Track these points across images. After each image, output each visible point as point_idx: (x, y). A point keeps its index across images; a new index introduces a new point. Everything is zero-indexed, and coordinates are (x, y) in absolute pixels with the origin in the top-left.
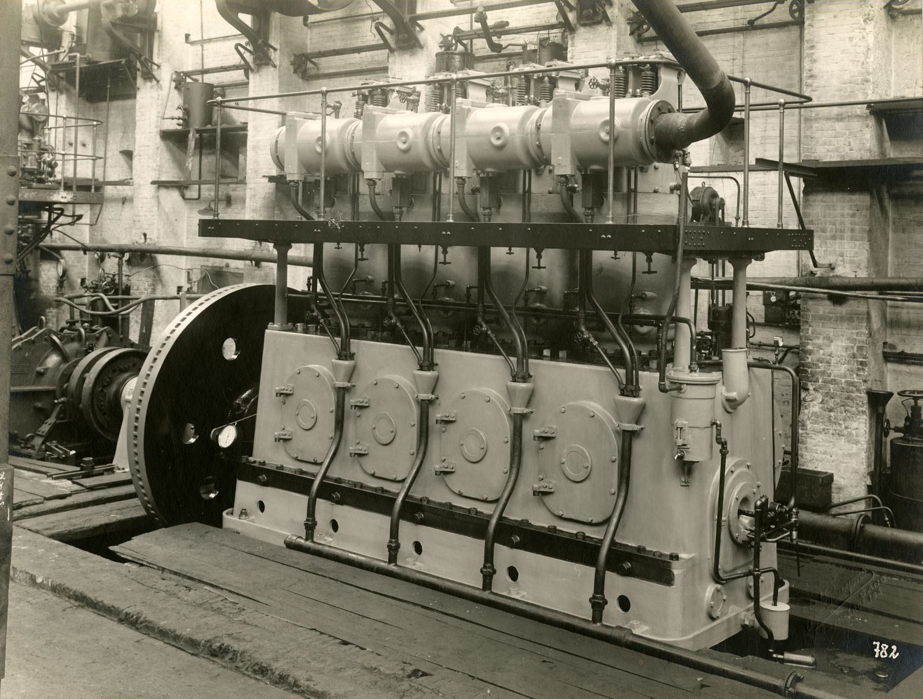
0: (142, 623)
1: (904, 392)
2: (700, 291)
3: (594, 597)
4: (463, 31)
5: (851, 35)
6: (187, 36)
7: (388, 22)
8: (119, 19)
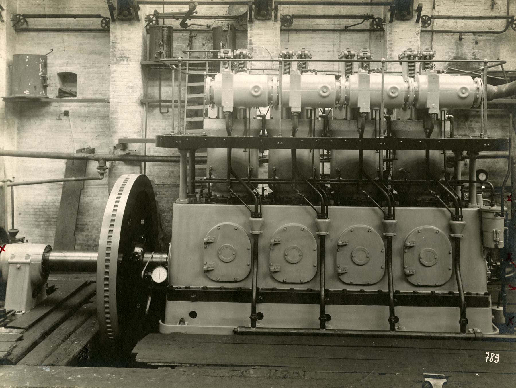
2: (324, 163)
3: (252, 315)
5: (411, 40)
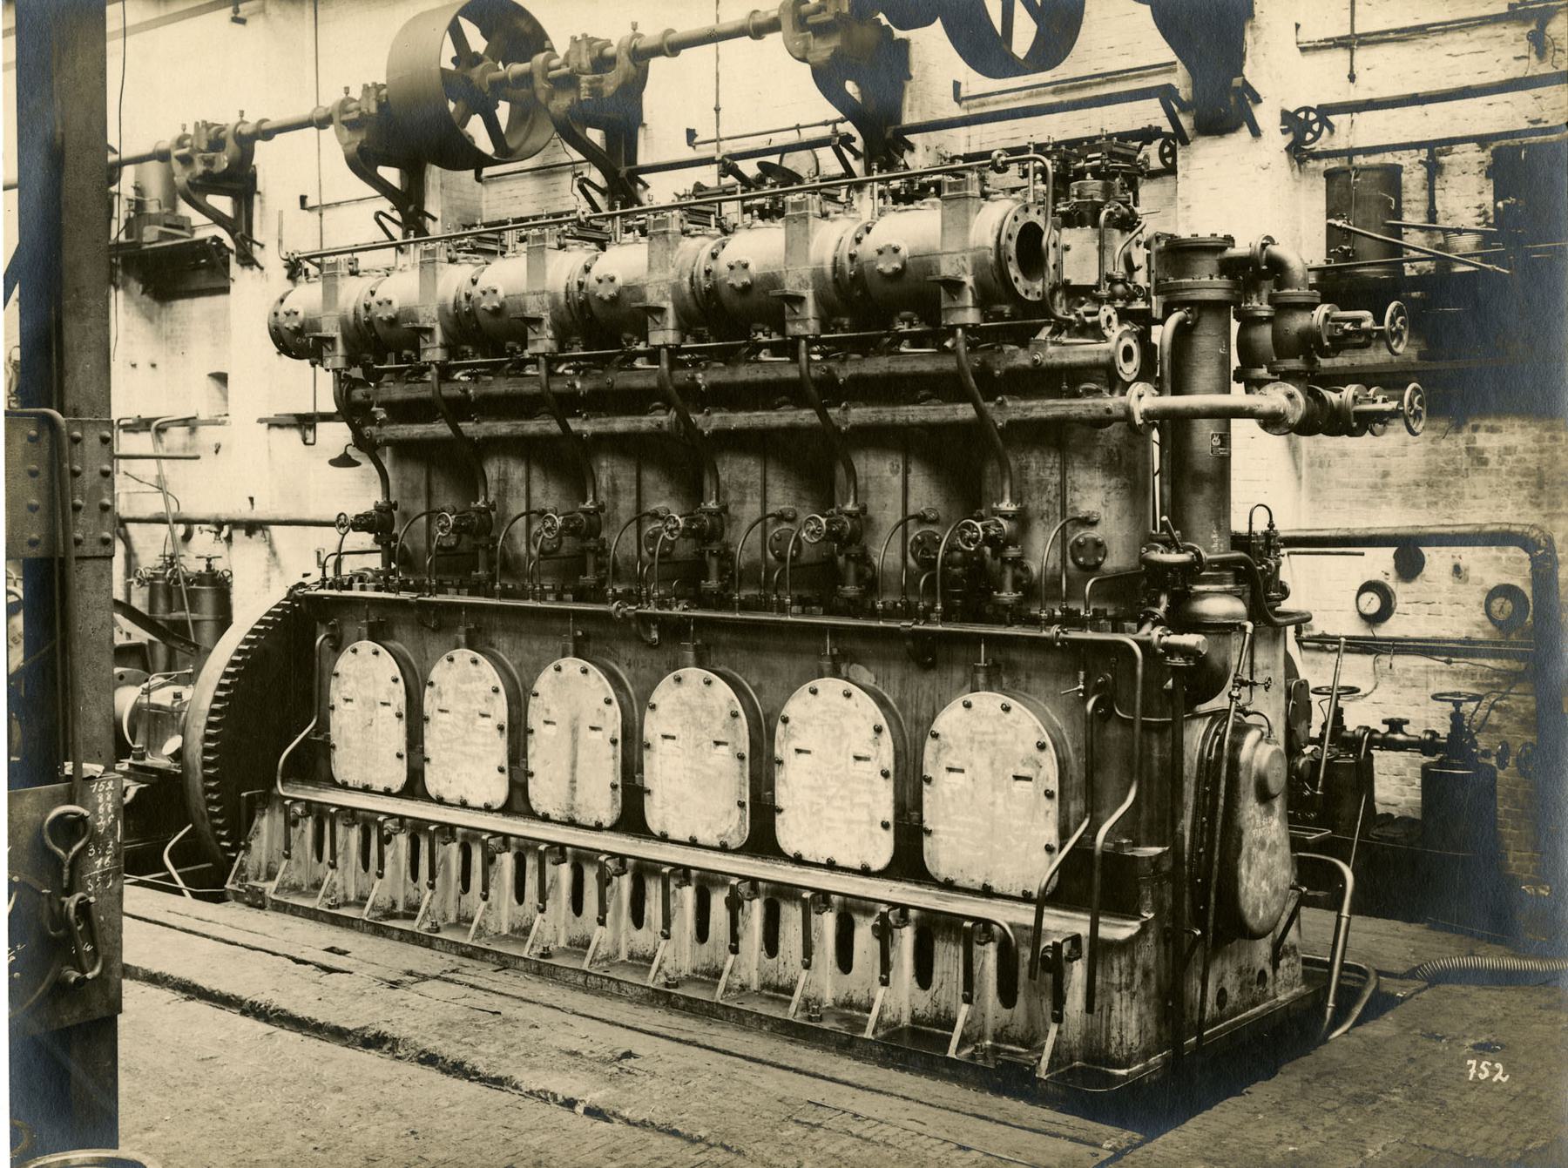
0: (272, 1012)
1: (1320, 688)
4: (707, 188)
6: (303, 199)
7: (596, 176)
8: (200, 177)
